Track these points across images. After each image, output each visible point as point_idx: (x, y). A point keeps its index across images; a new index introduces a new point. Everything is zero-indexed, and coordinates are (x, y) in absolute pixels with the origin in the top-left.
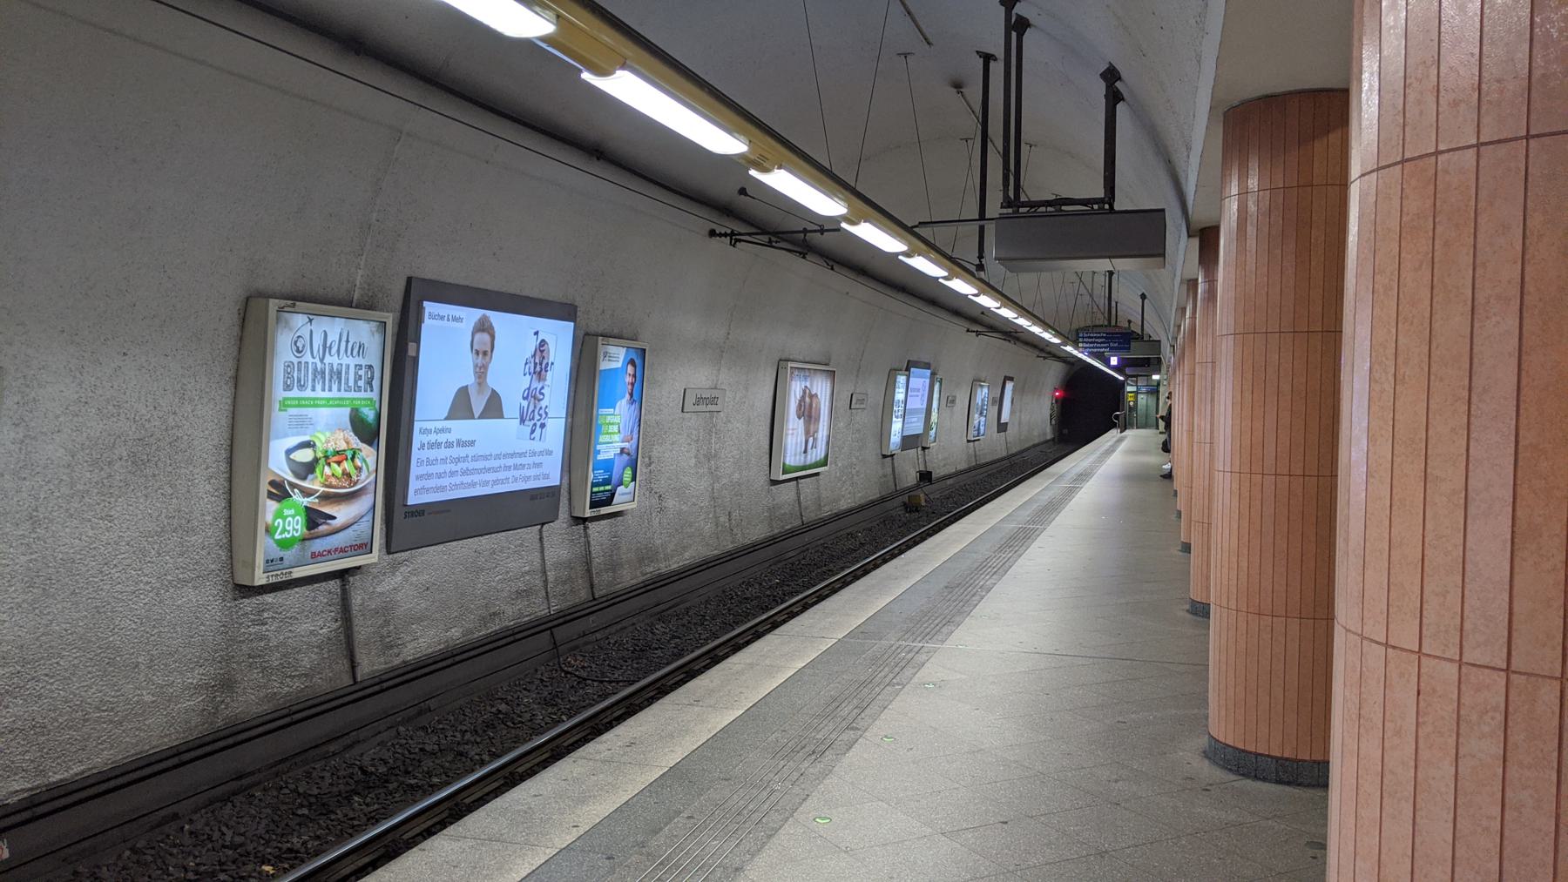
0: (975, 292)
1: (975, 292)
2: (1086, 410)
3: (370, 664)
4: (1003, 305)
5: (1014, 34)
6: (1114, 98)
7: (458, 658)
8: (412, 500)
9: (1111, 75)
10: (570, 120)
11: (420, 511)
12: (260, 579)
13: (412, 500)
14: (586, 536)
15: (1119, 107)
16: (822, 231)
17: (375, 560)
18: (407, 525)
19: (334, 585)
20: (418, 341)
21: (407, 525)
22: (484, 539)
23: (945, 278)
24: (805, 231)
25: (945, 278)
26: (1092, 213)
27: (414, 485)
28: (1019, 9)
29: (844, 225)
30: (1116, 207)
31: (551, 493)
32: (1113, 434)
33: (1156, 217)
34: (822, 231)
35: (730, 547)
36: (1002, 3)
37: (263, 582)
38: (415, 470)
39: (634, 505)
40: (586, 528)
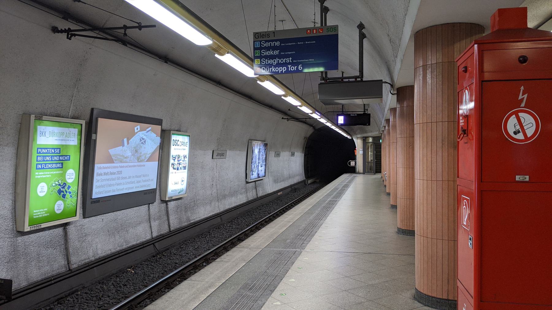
0: (311, 112)
1: (311, 112)
2: (327, 159)
3: (76, 261)
4: (416, 178)
5: (354, 80)
6: (362, 36)
7: (121, 255)
8: (94, 196)
9: (361, 27)
10: (218, 74)
11: (98, 200)
12: (27, 229)
13: (94, 196)
14: (167, 208)
15: (365, 41)
16: (140, 27)
17: (78, 219)
18: (91, 205)
19: (60, 230)
20: (96, 133)
21: (91, 205)
22: (118, 213)
23: (300, 106)
24: (125, 27)
25: (300, 106)
26: (356, 81)
27: (95, 190)
28: (326, 4)
29: (282, 97)
30: (364, 79)
31: (153, 191)
32: (344, 178)
33: (379, 84)
34: (140, 27)
35: (219, 212)
36: (319, 1)
37: (29, 230)
38: (95, 184)
39: (186, 195)
40: (167, 204)
